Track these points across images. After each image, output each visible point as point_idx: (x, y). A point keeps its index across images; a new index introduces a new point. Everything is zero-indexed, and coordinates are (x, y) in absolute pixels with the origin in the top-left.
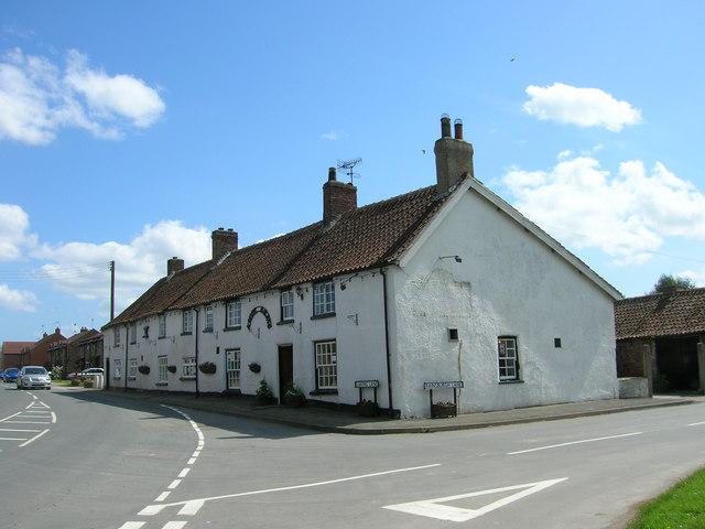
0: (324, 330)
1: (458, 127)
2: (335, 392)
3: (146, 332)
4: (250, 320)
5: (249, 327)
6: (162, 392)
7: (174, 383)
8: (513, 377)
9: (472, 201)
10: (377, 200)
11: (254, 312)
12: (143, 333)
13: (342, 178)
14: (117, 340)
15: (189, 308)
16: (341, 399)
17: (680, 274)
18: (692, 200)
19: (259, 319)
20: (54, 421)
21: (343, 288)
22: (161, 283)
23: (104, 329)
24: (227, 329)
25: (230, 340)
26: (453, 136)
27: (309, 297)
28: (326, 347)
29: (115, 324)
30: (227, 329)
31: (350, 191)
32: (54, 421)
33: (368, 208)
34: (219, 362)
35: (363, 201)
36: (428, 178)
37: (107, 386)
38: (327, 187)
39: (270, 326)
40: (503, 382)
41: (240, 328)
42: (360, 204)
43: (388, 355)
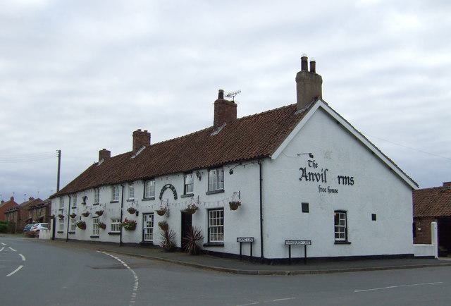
1: (313, 63)
2: (222, 245)
3: (85, 201)
4: (162, 194)
5: (161, 198)
6: (94, 242)
7: (104, 237)
8: (344, 239)
9: (321, 116)
10: (189, 133)
11: (164, 189)
12: (82, 201)
15: (117, 184)
16: (227, 250)
17: (349, 215)
18: (300, 179)
19: (169, 193)
20: (24, 259)
21: (231, 173)
22: (94, 168)
23: (53, 197)
24: (144, 199)
26: (309, 70)
27: (205, 178)
29: (60, 194)
30: (144, 199)
31: (233, 106)
32: (24, 259)
33: (243, 119)
36: (290, 98)
37: (53, 238)
38: (216, 103)
39: (176, 198)
40: (337, 243)
41: (154, 199)
42: (239, 116)
43: (262, 220)
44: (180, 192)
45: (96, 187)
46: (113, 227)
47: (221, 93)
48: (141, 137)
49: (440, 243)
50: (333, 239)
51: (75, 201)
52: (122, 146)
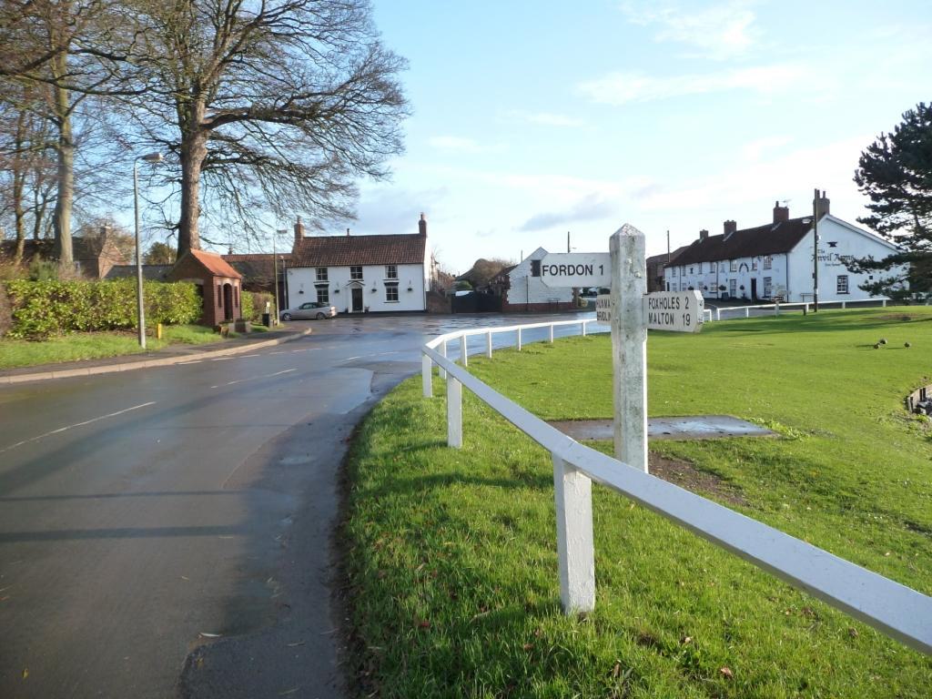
0: (767, 274)
1: (824, 193)
9: (828, 223)
11: (742, 265)
13: (781, 205)
14: (674, 273)
19: (744, 268)
25: (732, 276)
28: (767, 280)
31: (786, 211)
33: (739, 231)
34: (727, 285)
35: (792, 216)
44: (750, 268)
45: (700, 261)
46: (712, 288)
47: (777, 203)
48: (730, 226)
49: (212, 286)
50: (836, 291)
51: (684, 271)
52: (717, 230)
